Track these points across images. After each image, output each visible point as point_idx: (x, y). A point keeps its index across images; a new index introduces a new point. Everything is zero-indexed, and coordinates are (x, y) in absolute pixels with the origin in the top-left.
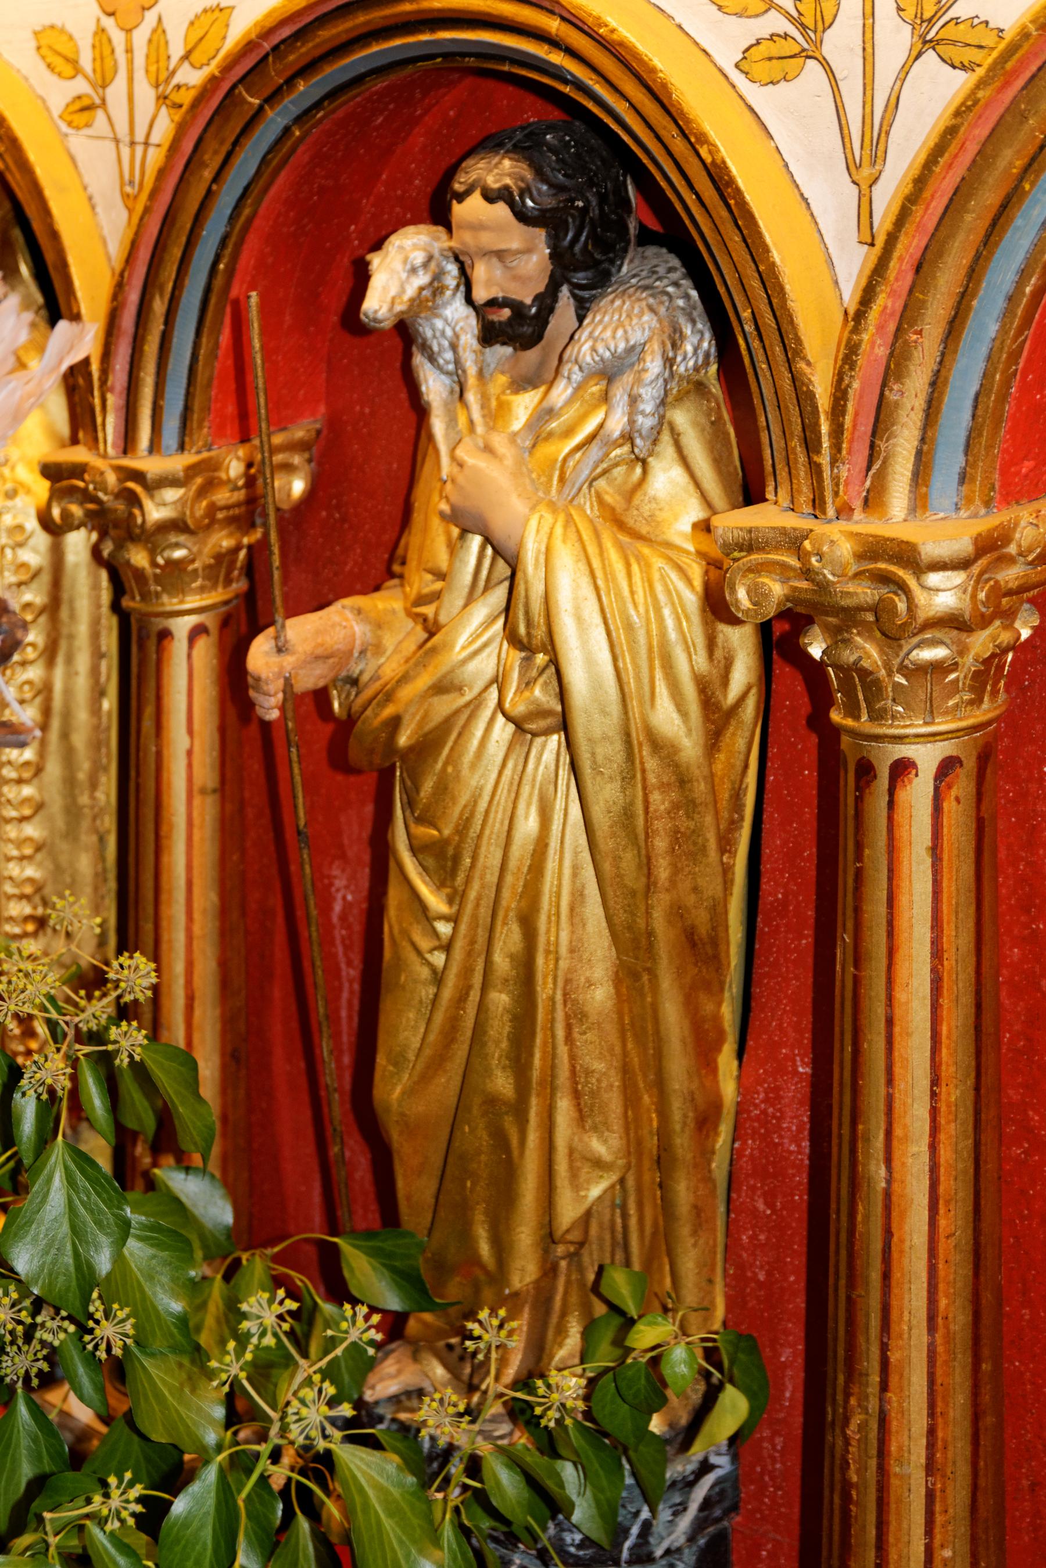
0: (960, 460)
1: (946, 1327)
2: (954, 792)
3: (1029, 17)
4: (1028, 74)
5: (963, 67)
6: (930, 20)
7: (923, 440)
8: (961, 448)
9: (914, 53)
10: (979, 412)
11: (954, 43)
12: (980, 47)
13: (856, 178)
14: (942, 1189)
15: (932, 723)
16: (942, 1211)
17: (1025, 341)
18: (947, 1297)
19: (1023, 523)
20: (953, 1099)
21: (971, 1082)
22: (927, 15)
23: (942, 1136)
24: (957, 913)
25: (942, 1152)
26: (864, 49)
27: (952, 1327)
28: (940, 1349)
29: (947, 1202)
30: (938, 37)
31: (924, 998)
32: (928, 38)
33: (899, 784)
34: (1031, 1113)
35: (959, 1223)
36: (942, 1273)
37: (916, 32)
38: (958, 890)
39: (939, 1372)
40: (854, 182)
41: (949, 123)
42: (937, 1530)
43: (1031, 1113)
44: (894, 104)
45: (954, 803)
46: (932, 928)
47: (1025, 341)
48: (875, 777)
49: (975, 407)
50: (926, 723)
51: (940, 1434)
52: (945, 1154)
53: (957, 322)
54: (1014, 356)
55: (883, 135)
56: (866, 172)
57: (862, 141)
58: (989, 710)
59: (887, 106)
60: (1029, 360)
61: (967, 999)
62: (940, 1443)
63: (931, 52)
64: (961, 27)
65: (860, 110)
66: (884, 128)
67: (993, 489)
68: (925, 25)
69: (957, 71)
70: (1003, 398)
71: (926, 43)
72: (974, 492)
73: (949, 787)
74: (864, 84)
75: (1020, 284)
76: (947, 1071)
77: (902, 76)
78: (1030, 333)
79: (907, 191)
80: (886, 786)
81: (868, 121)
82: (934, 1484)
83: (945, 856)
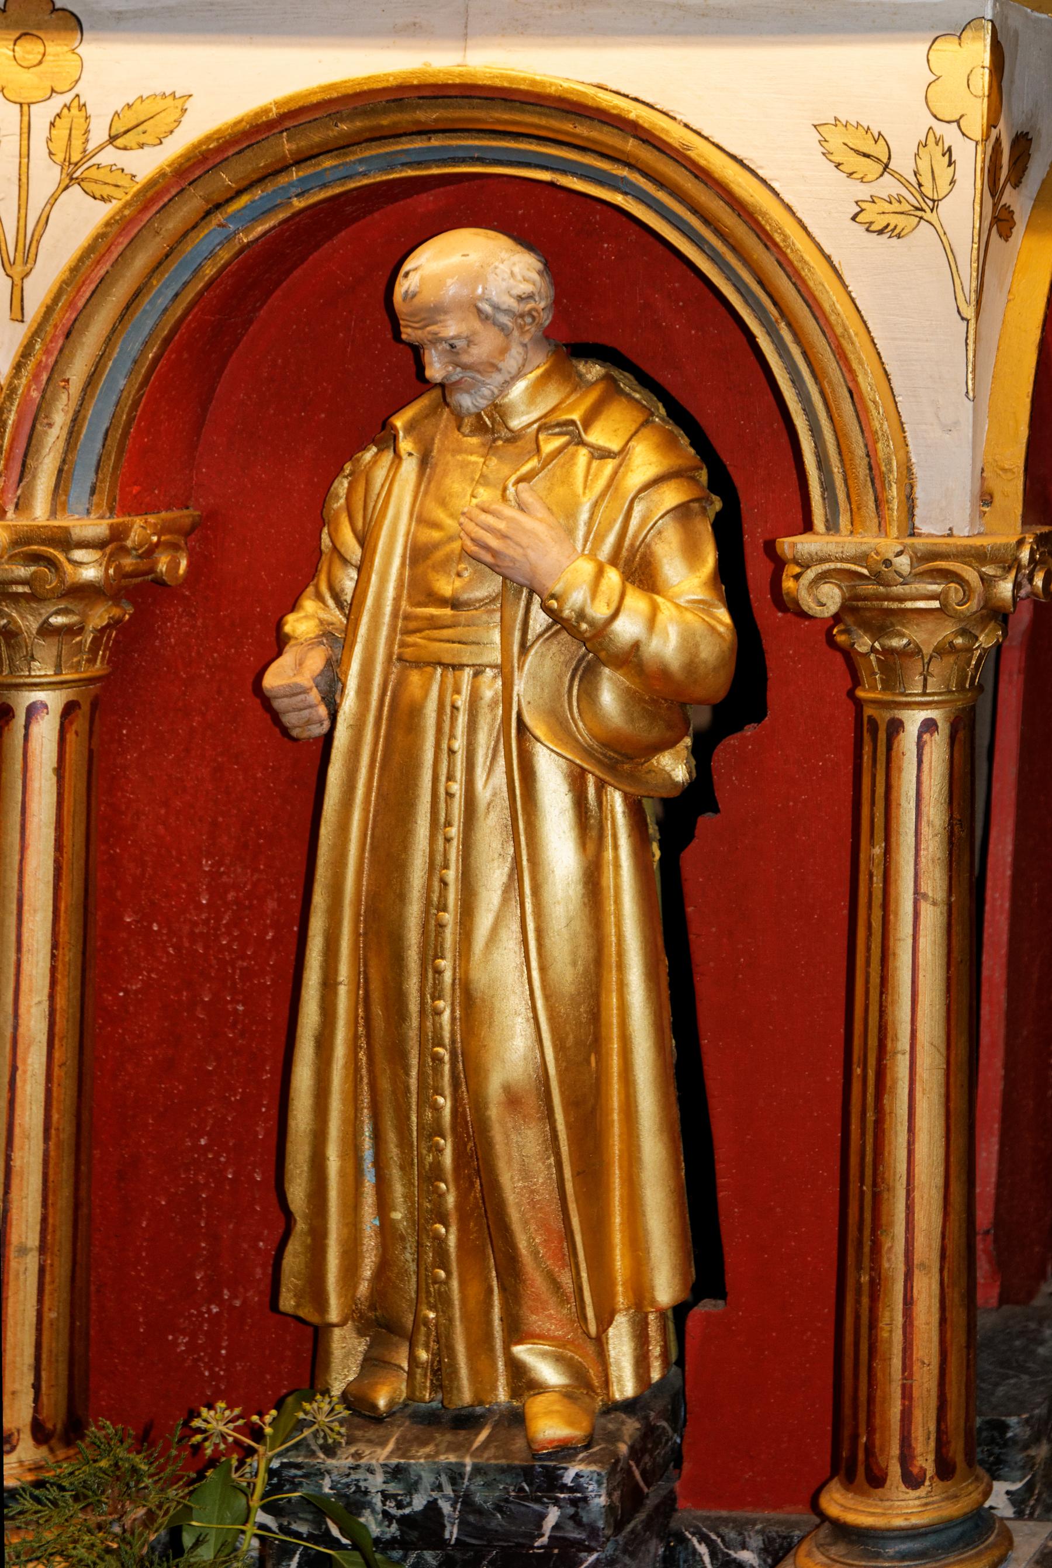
0: (91, 477)
1: (58, 1136)
2: (74, 728)
3: (166, 163)
4: (161, 204)
5: (103, 199)
6: (76, 164)
7: (64, 461)
8: (93, 469)
9: (62, 186)
10: (108, 442)
11: (96, 181)
12: (117, 186)
13: (9, 272)
14: (57, 1029)
15: (61, 674)
16: (56, 1047)
17: (143, 395)
18: (58, 1113)
19: (135, 526)
20: (67, 959)
21: (80, 947)
22: (74, 160)
23: (59, 988)
24: (74, 817)
25: (58, 999)
26: (20, 180)
27: (61, 1136)
28: (52, 1154)
29: (61, 1040)
30: (83, 176)
31: (48, 882)
32: (75, 176)
33: (33, 722)
34: (105, 995)
35: (69, 1055)
36: (55, 1094)
37: (65, 171)
38: (75, 800)
39: (51, 1172)
40: (8, 275)
41: (100, 231)
42: (46, 1297)
43: (105, 995)
44: (44, 221)
45: (74, 736)
46: (56, 829)
47: (143, 395)
48: (14, 717)
49: (105, 439)
50: (56, 674)
51: (50, 1221)
52: (61, 1002)
53: (95, 376)
54: (136, 404)
55: (34, 242)
56: (18, 269)
57: (16, 245)
58: (98, 670)
59: (38, 222)
60: (143, 410)
61: (79, 884)
62: (50, 1226)
63: (76, 186)
64: (102, 170)
65: (15, 223)
66: (36, 237)
67: (115, 500)
68: (72, 167)
69: (98, 202)
70: (125, 434)
71: (71, 180)
72: (103, 500)
73: (71, 723)
74: (19, 206)
75: (143, 352)
76: (63, 938)
77: (52, 201)
78: (147, 389)
79: (64, 277)
80: (23, 723)
81: (22, 231)
82: (45, 1261)
83: (67, 774)
